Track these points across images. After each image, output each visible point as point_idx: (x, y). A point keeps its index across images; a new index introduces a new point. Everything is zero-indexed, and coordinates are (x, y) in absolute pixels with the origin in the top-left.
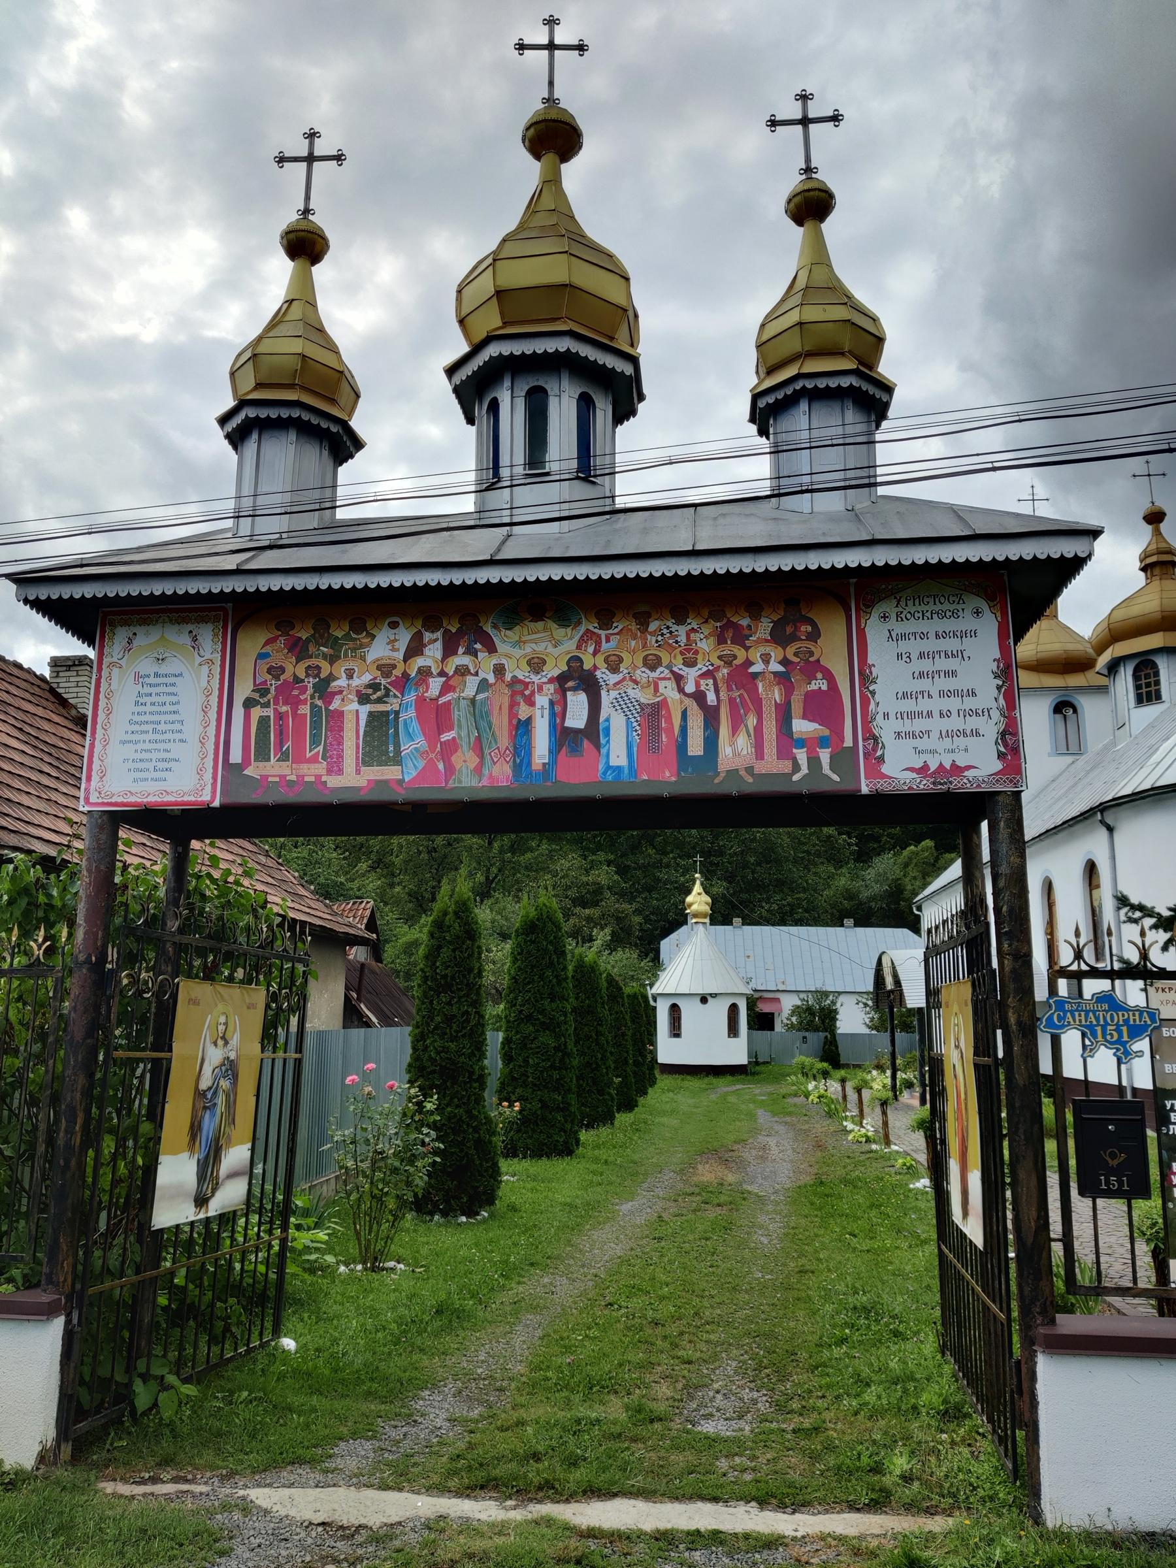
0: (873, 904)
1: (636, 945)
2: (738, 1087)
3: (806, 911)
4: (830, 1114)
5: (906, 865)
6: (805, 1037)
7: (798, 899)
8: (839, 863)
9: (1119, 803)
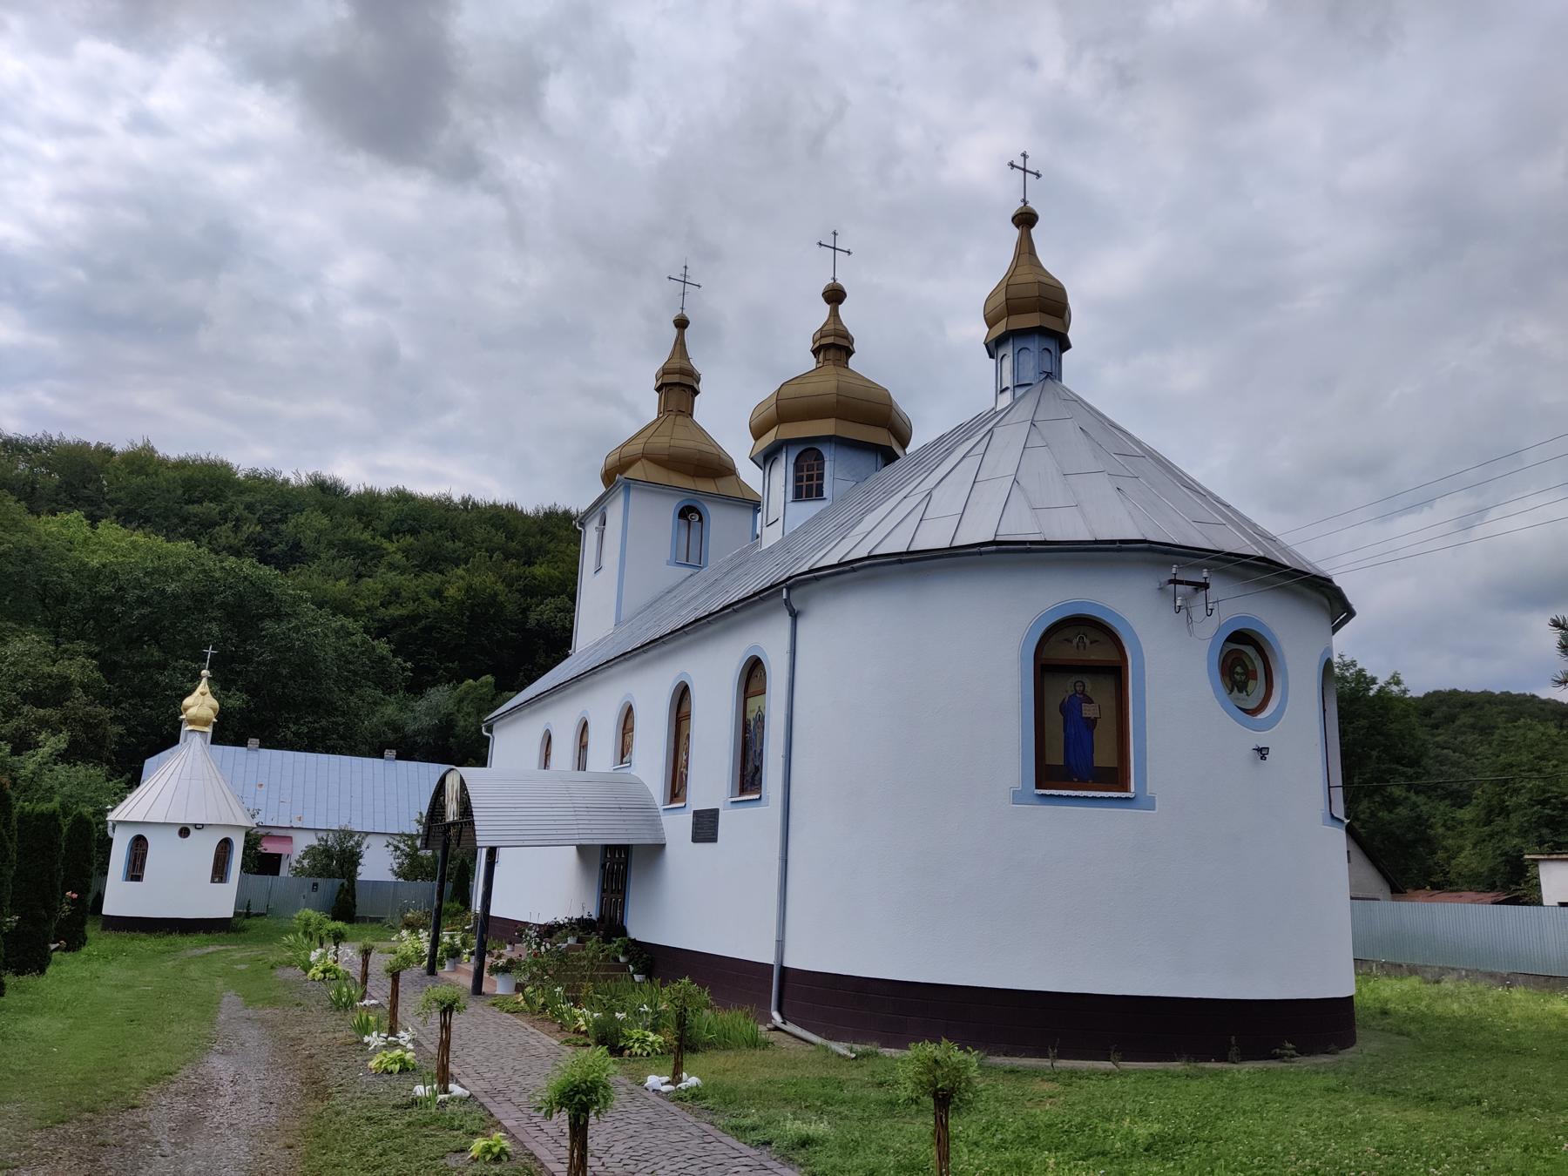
0: (419, 739)
1: (109, 762)
2: (211, 949)
3: (342, 737)
4: (343, 1006)
5: (461, 700)
6: (315, 885)
7: (336, 723)
8: (389, 690)
9: (816, 576)
